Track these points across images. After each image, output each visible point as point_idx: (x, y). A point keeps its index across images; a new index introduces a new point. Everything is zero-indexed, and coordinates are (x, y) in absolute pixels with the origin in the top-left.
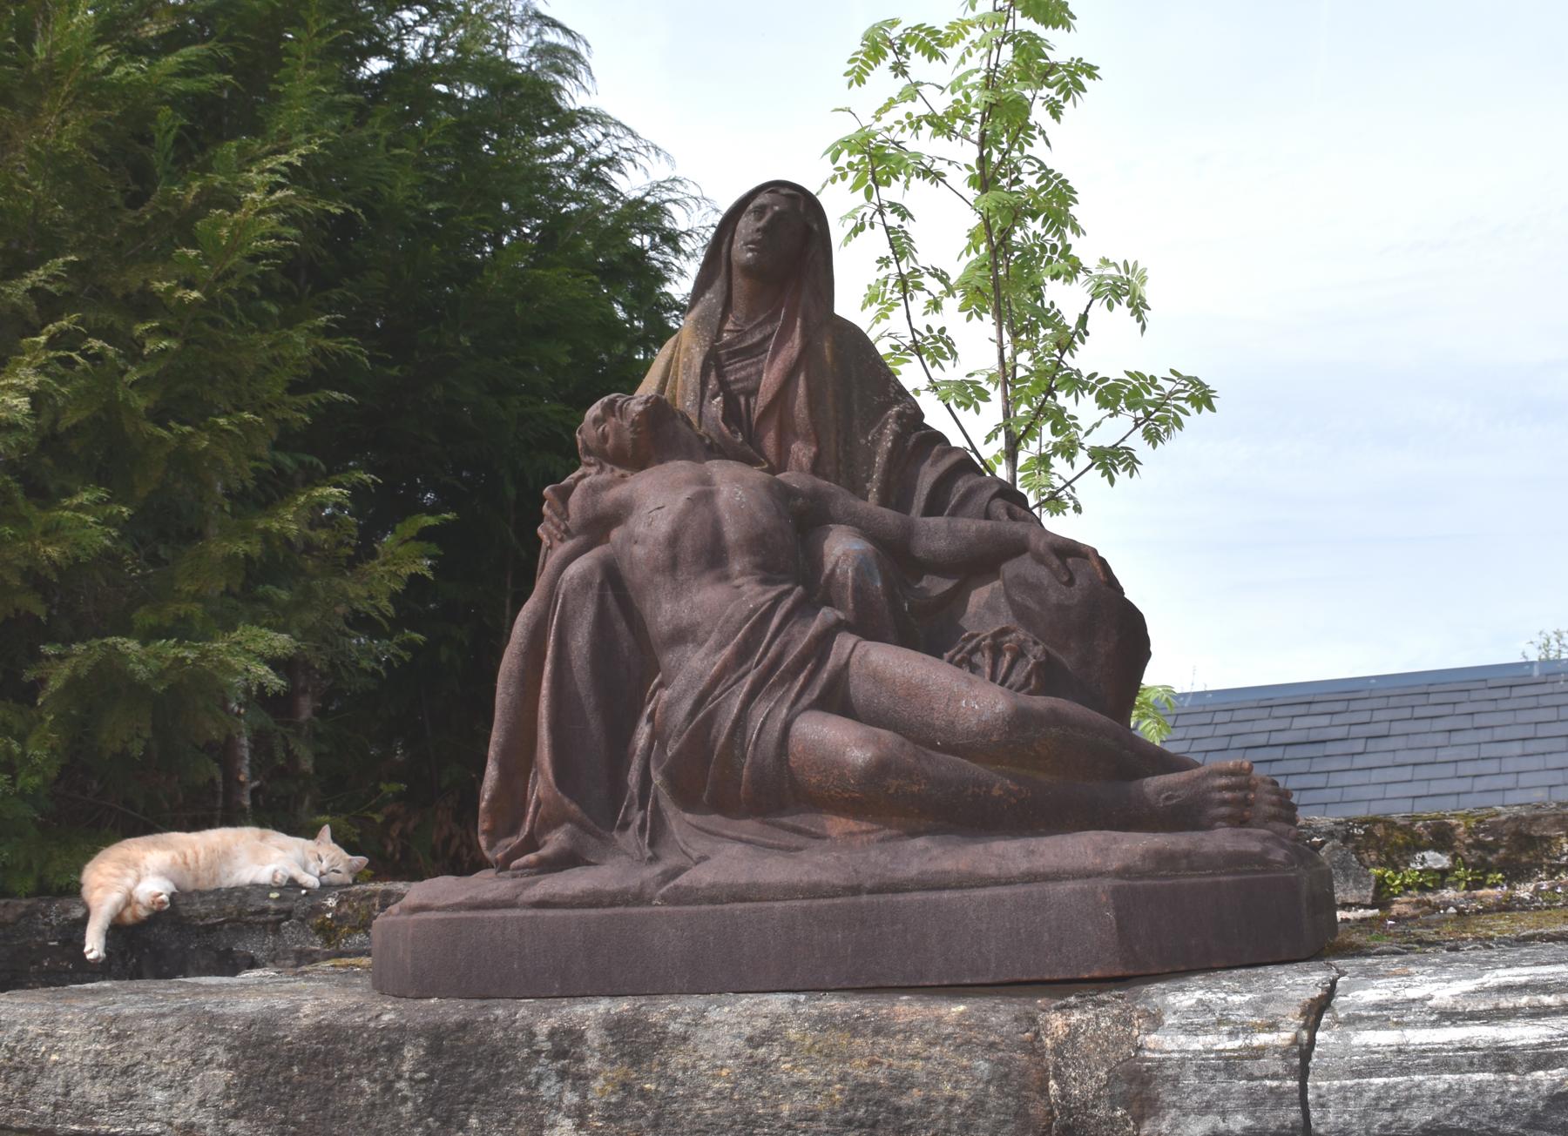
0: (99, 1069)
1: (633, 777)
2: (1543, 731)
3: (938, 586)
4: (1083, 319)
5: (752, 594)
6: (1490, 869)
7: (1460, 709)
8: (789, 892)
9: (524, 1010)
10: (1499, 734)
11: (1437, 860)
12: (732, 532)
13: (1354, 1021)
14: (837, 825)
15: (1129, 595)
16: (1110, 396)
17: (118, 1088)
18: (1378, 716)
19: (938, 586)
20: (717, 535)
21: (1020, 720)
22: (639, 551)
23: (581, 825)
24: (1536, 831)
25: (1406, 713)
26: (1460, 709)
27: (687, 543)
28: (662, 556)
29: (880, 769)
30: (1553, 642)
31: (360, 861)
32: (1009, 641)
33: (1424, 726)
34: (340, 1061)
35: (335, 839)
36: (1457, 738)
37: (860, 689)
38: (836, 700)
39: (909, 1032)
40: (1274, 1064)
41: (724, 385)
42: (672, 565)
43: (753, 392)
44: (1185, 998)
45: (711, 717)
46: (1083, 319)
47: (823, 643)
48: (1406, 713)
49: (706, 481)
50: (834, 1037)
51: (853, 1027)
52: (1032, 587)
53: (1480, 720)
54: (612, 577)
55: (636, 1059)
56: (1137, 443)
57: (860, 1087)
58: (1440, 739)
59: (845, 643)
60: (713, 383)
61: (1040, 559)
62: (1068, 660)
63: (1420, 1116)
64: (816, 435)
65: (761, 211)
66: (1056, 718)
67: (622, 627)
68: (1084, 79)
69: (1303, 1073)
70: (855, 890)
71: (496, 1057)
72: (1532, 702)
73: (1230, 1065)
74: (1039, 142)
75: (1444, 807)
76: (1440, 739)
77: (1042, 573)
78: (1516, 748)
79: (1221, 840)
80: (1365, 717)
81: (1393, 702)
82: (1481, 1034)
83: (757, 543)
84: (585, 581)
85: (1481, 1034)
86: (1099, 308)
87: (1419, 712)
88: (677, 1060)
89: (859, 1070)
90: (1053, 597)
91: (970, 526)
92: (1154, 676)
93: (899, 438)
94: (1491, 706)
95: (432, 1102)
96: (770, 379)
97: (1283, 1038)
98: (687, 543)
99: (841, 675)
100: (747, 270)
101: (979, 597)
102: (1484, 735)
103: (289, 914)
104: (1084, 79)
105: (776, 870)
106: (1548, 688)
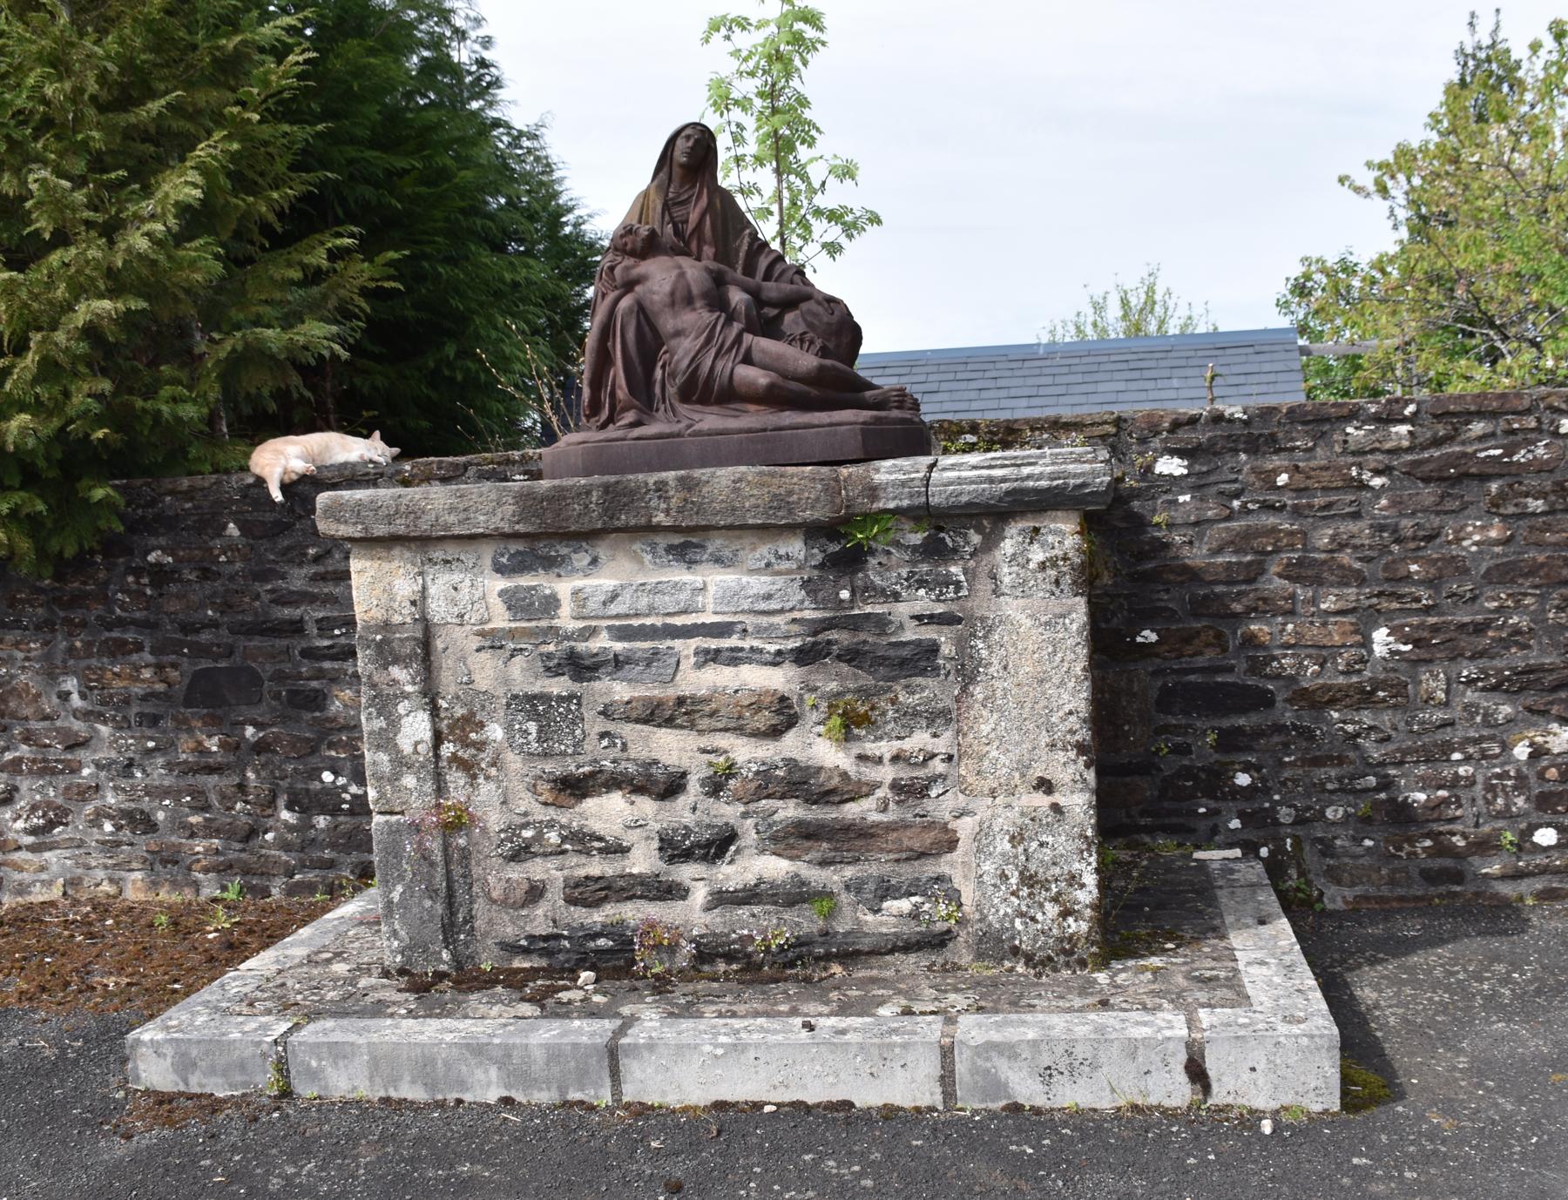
0: (452, 509)
1: (657, 390)
2: (1042, 391)
3: (773, 312)
4: (823, 184)
5: (707, 317)
6: (994, 443)
7: (988, 375)
8: (740, 431)
9: (641, 476)
10: (1013, 392)
11: (971, 438)
12: (695, 291)
13: (944, 469)
14: (752, 408)
15: (856, 319)
16: (833, 216)
17: (462, 516)
18: (931, 378)
19: (773, 312)
20: (690, 292)
21: (821, 368)
22: (656, 298)
23: (640, 410)
24: (1016, 426)
25: (951, 376)
26: (988, 375)
27: (678, 295)
28: (667, 300)
29: (771, 387)
30: (1059, 328)
31: (396, 450)
32: (808, 336)
33: (963, 385)
34: (565, 498)
35: (382, 438)
36: (984, 394)
37: (756, 356)
38: (748, 360)
39: (792, 476)
40: (917, 483)
41: (672, 219)
42: (673, 304)
43: (687, 221)
44: (888, 463)
45: (697, 367)
46: (823, 184)
47: (738, 340)
48: (951, 376)
49: (680, 267)
50: (765, 478)
51: (772, 475)
52: (815, 315)
53: (1001, 383)
54: (641, 309)
55: (690, 490)
56: (843, 240)
57: (775, 495)
58: (973, 395)
59: (748, 338)
60: (667, 218)
61: (819, 303)
62: (831, 345)
63: (964, 499)
64: (715, 243)
65: (688, 137)
66: (834, 368)
67: (647, 329)
68: (819, 46)
69: (927, 486)
70: (765, 430)
71: (632, 493)
72: (1037, 372)
73: (903, 484)
74: (796, 80)
75: (977, 417)
76: (973, 395)
77: (820, 309)
78: (1024, 402)
79: (895, 413)
80: (922, 378)
81: (942, 368)
82: (985, 472)
83: (705, 295)
84: (630, 310)
85: (985, 472)
86: (831, 177)
87: (959, 376)
88: (705, 490)
89: (774, 490)
90: (825, 319)
91: (786, 287)
92: (862, 351)
93: (751, 245)
94: (1009, 373)
95: (606, 510)
96: (694, 217)
97: (921, 475)
98: (678, 295)
99: (749, 351)
100: (682, 166)
101: (789, 317)
102: (1003, 393)
103: (382, 475)
104: (819, 46)
105: (732, 424)
106: (1048, 363)
